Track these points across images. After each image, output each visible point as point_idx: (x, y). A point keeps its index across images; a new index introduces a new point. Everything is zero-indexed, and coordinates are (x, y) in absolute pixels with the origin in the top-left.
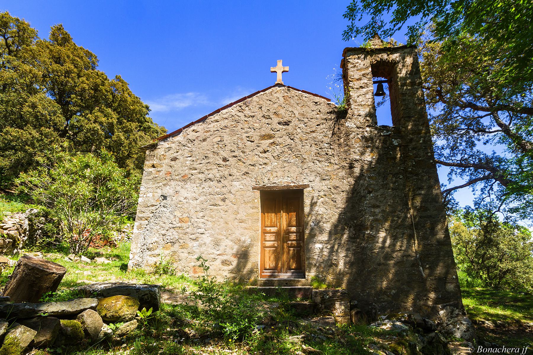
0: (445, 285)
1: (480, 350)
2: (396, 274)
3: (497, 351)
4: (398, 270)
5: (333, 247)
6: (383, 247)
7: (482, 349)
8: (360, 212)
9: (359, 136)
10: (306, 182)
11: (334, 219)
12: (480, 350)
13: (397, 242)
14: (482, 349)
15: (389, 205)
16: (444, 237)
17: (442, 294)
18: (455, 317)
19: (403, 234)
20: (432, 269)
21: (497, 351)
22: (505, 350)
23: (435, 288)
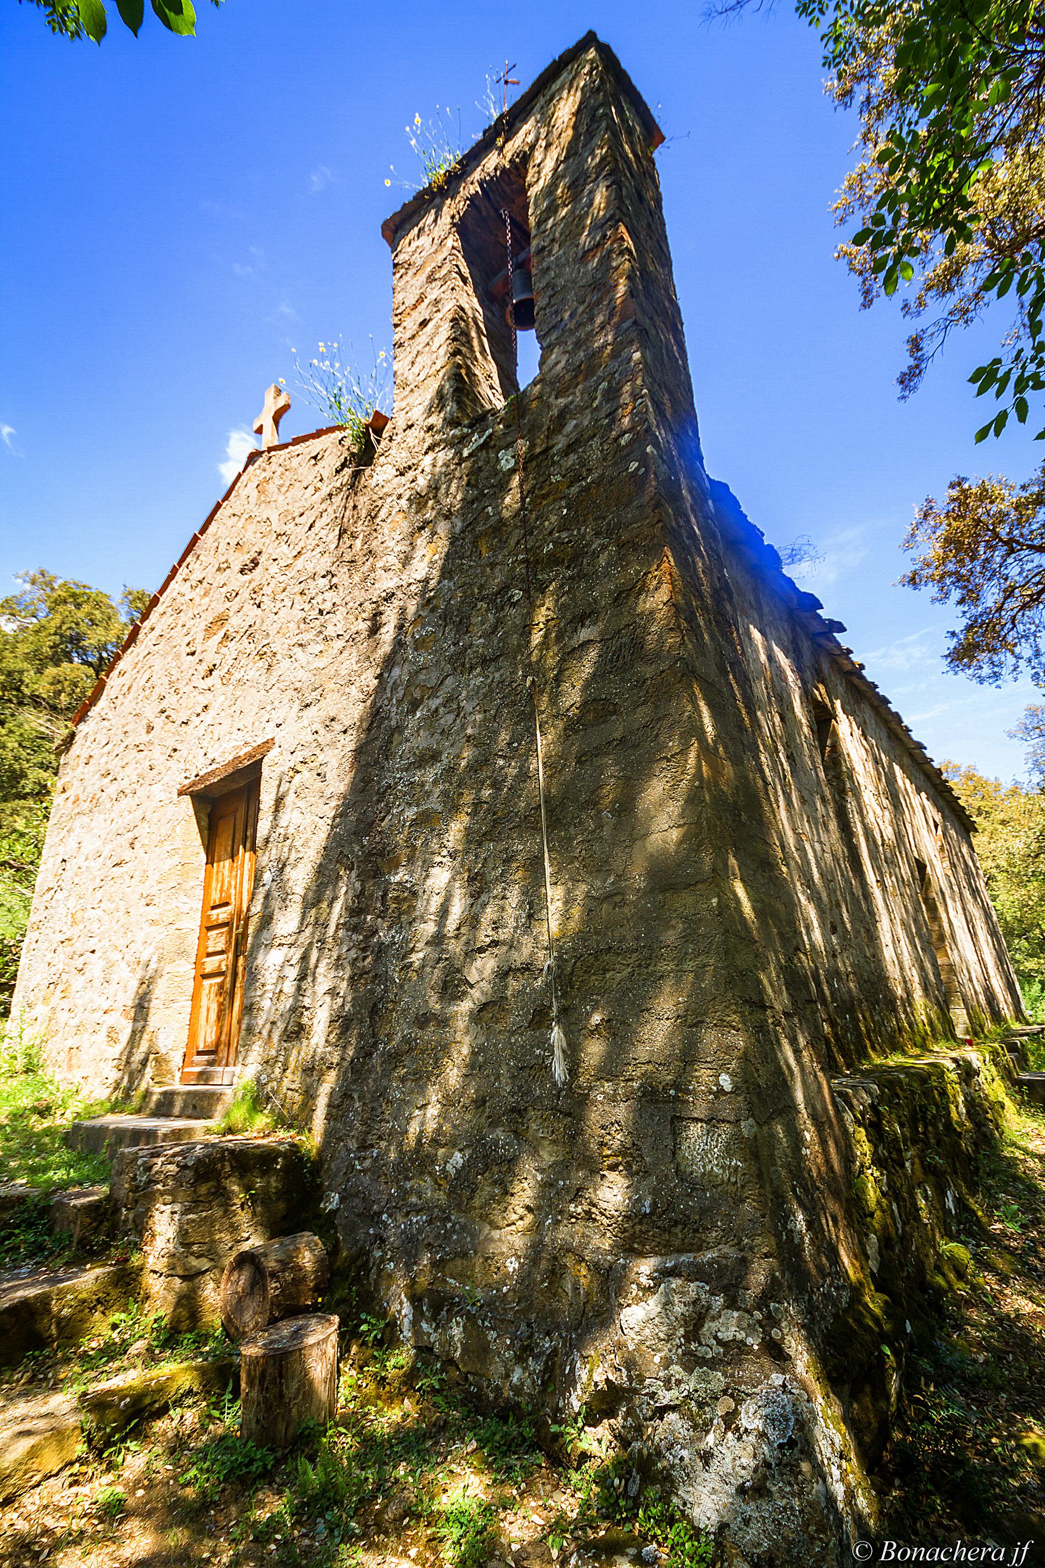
0: (675, 1134)
1: (888, 1555)
2: (474, 1067)
3: (940, 1555)
4: (482, 1049)
5: (305, 958)
6: (438, 940)
7: (896, 1551)
8: (382, 795)
9: (404, 503)
10: (270, 731)
11: (321, 838)
12: (888, 1555)
13: (485, 905)
14: (896, 1551)
15: (469, 738)
16: (681, 842)
17: (655, 1192)
18: (713, 1364)
19: (507, 861)
20: (620, 1033)
21: (940, 1555)
22: (961, 1553)
23: (622, 1152)
